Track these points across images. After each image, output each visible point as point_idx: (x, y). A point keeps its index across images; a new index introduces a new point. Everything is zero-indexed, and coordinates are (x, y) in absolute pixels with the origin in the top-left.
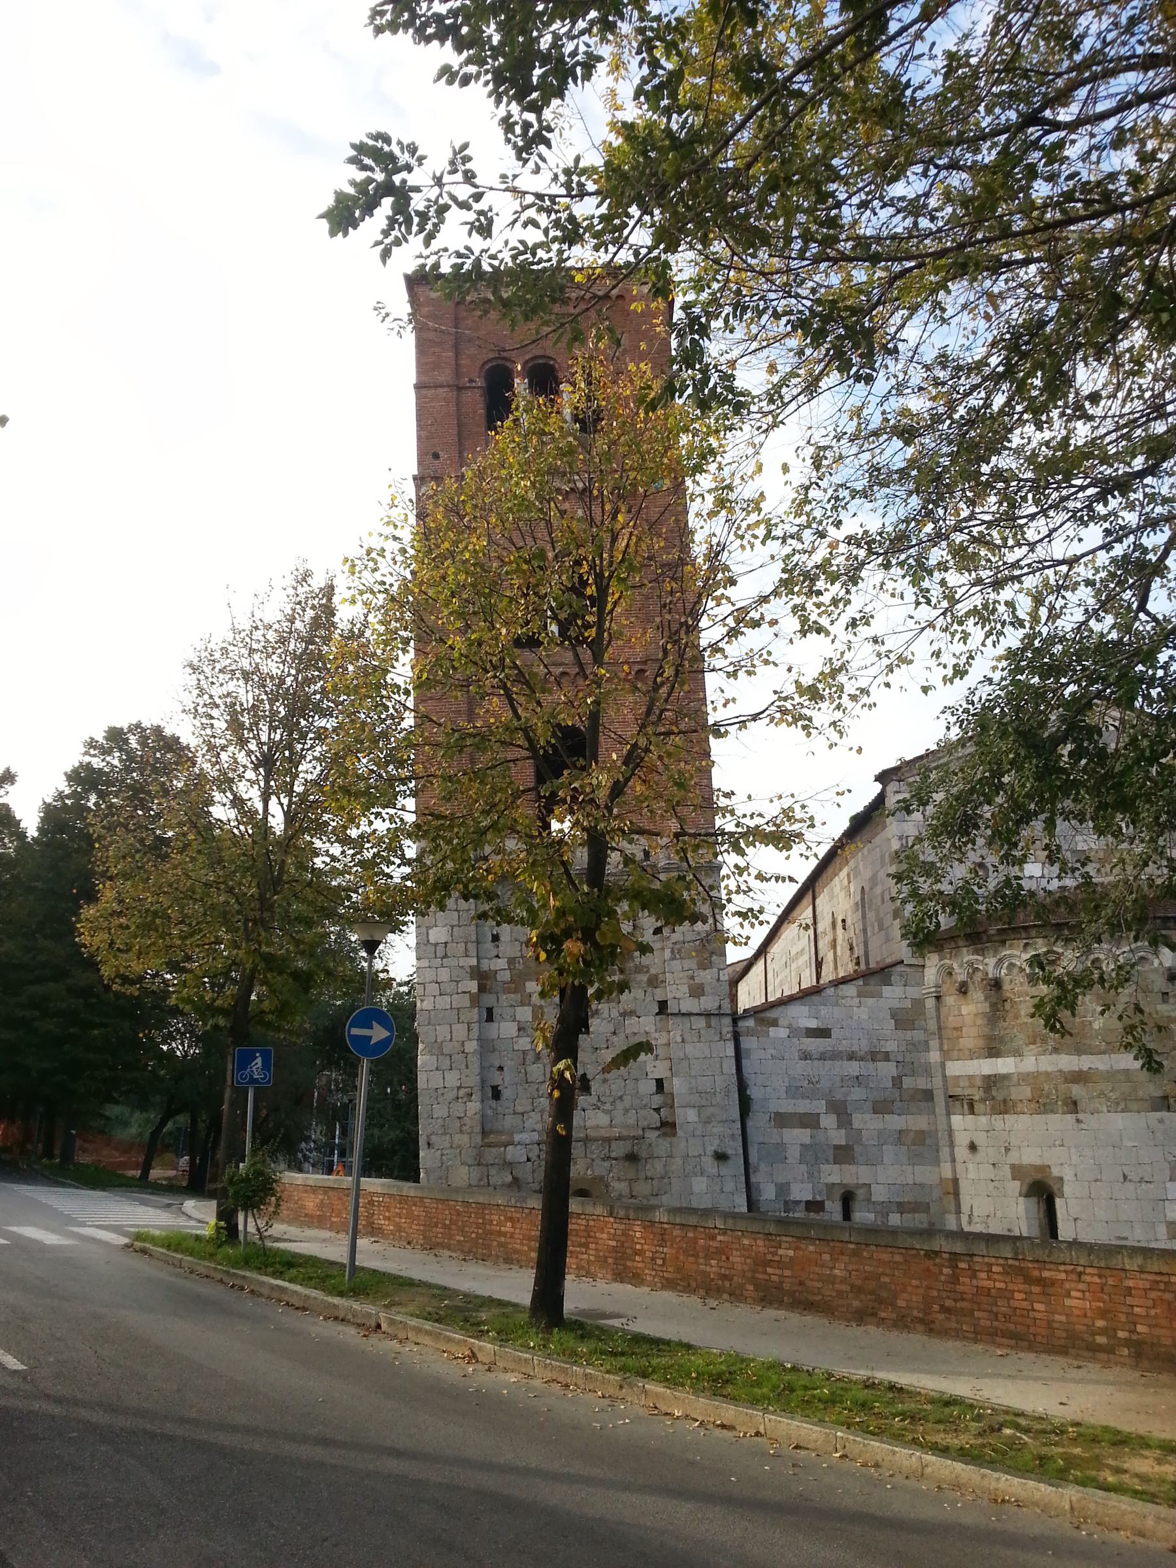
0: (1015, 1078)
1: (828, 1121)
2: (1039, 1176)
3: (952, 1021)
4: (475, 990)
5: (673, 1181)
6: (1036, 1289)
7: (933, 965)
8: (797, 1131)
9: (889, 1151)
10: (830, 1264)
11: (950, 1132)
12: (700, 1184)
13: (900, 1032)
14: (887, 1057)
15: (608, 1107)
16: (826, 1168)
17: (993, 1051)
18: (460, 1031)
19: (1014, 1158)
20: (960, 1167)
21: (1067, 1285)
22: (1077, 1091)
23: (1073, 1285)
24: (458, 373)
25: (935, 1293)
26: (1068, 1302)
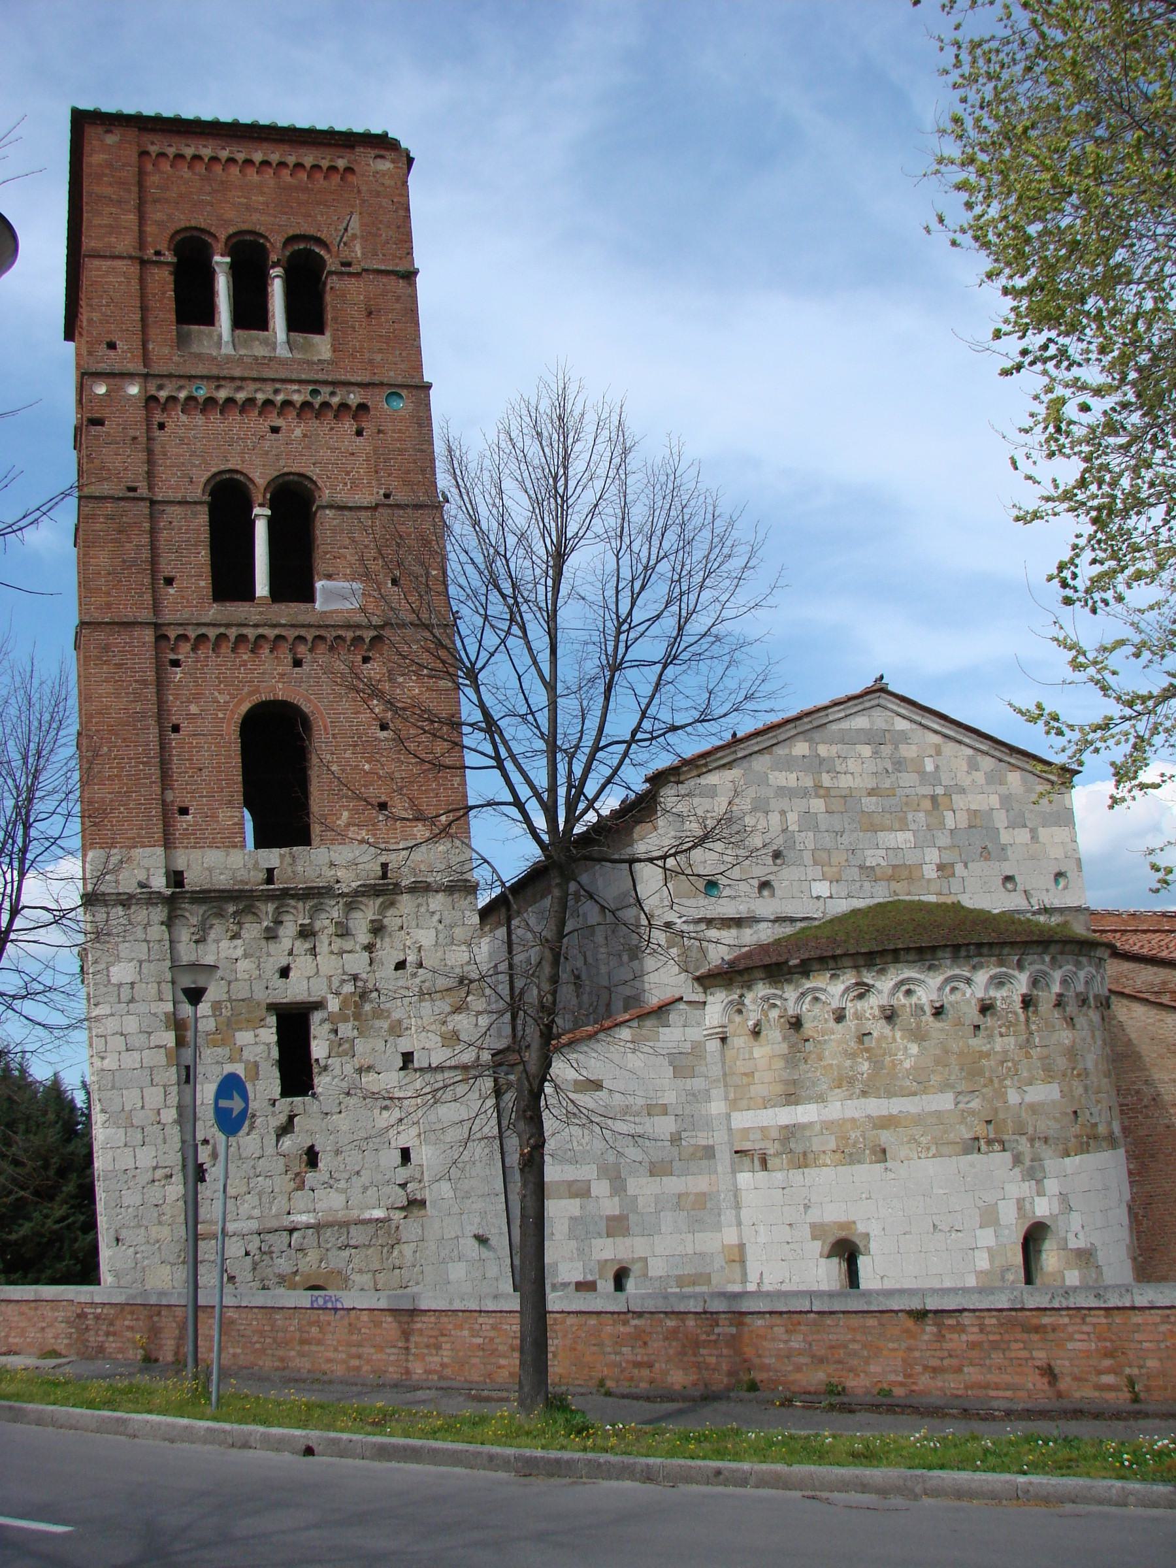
0: (818, 1127)
1: (600, 1188)
2: (843, 1234)
3: (741, 1067)
4: (171, 1043)
5: (427, 1269)
6: (1035, 1337)
7: (717, 1004)
8: (564, 1202)
9: (668, 1220)
10: (785, 1337)
11: (736, 1192)
12: (457, 1272)
13: (680, 1082)
14: (664, 1110)
15: (342, 1184)
16: (598, 1243)
17: (791, 1098)
18: (154, 1097)
19: (814, 1216)
20: (747, 1232)
21: (1070, 1329)
22: (886, 1137)
23: (1076, 1328)
24: (142, 244)
25: (917, 1354)
26: (1070, 1346)
